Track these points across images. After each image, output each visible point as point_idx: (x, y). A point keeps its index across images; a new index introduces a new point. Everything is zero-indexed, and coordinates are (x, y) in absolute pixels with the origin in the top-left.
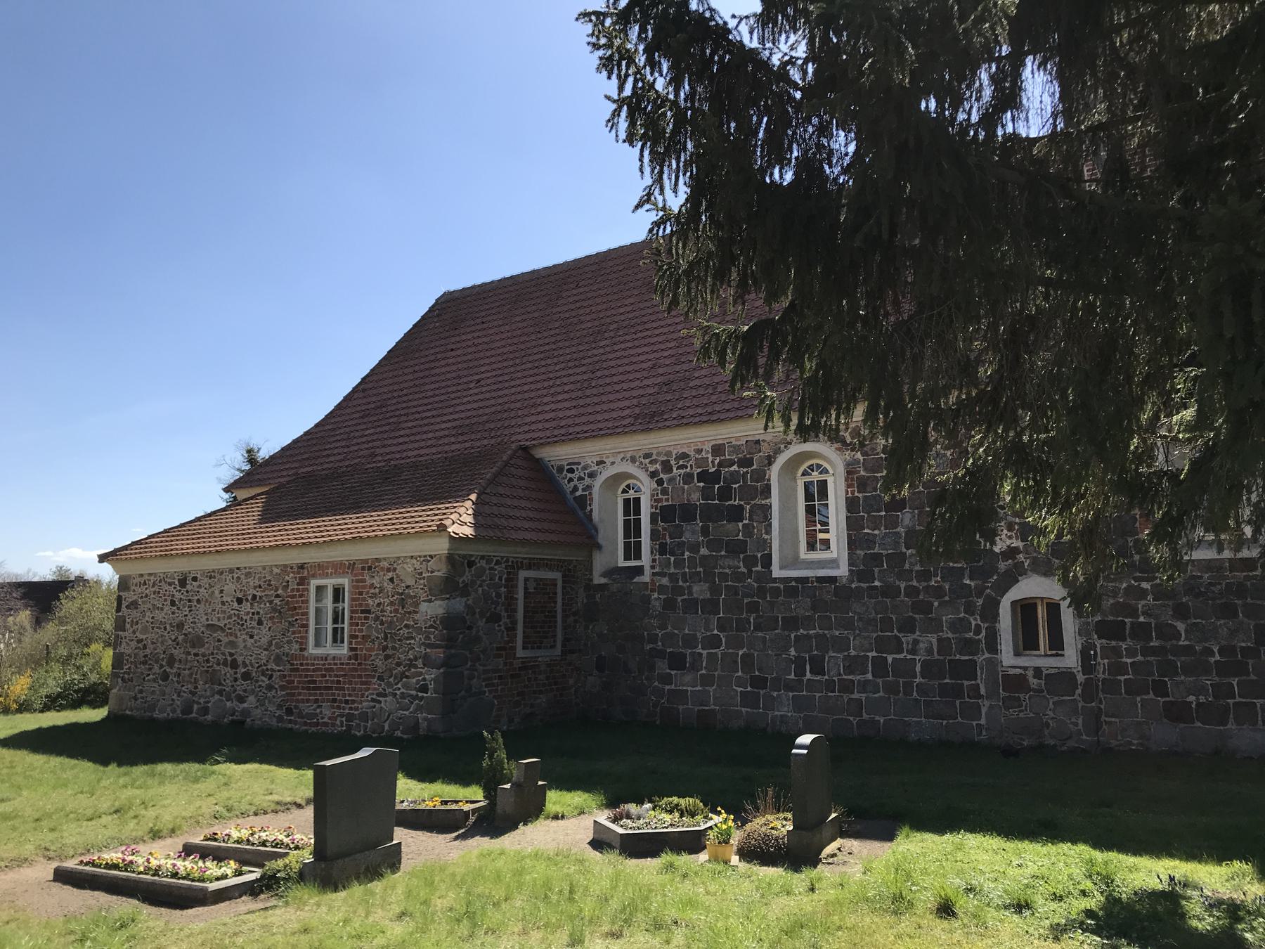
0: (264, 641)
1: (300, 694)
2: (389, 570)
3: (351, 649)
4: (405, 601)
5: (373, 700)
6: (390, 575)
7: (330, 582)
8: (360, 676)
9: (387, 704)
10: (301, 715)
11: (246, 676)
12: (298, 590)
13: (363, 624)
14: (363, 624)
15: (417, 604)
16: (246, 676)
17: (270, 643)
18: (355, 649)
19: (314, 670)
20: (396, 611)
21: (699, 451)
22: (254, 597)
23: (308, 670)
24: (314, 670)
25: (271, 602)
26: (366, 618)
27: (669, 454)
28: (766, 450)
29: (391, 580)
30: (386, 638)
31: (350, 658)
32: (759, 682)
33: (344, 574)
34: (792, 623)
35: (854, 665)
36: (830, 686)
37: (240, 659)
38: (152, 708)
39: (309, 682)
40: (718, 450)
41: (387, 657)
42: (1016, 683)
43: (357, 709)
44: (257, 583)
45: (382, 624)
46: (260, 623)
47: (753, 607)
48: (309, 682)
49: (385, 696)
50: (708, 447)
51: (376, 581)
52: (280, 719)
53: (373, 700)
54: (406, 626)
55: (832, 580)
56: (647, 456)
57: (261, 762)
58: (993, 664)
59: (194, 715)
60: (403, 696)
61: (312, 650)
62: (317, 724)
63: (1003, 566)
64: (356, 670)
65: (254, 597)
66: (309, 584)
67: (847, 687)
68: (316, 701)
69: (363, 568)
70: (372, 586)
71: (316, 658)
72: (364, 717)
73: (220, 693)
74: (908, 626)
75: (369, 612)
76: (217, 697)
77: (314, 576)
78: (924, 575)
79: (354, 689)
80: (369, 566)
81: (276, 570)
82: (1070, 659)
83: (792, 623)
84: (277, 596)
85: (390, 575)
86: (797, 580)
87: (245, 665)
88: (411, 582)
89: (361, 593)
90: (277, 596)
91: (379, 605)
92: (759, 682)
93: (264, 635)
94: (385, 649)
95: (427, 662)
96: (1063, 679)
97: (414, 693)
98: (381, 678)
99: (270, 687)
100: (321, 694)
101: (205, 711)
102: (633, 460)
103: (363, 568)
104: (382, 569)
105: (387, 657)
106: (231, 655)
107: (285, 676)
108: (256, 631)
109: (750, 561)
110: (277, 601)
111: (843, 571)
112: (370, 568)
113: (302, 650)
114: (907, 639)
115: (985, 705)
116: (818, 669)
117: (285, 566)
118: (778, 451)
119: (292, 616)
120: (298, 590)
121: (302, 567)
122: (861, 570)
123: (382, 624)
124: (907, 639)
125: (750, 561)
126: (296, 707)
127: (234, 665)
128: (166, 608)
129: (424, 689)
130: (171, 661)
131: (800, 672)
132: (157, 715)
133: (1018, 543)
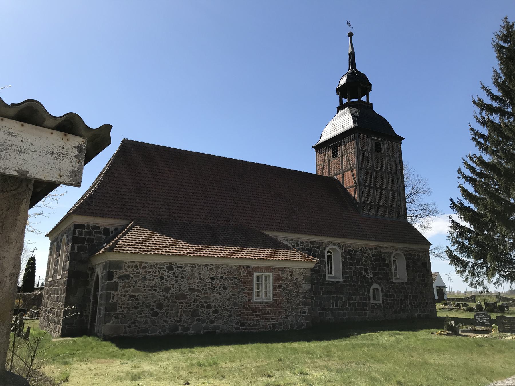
0: (228, 296)
1: (248, 317)
2: (290, 272)
3: (274, 299)
4: (295, 282)
5: (284, 318)
6: (290, 273)
7: (263, 275)
8: (278, 309)
9: (290, 318)
10: (249, 325)
11: (216, 312)
12: (247, 276)
13: (279, 290)
14: (279, 290)
15: (300, 284)
16: (216, 312)
17: (231, 297)
18: (276, 299)
19: (256, 308)
20: (293, 286)
21: (307, 242)
22: (222, 278)
23: (253, 308)
24: (256, 308)
25: (232, 280)
26: (280, 288)
27: (298, 241)
28: (324, 245)
29: (291, 275)
30: (288, 295)
31: (273, 303)
32: (323, 309)
33: (270, 272)
34: (331, 293)
35: (344, 304)
36: (339, 309)
37: (213, 305)
38: (145, 330)
39: (253, 312)
40: (312, 243)
41: (288, 302)
42: (373, 307)
43: (276, 321)
44: (223, 272)
45: (287, 290)
46: (225, 288)
47: (322, 289)
48: (253, 312)
49: (289, 316)
50: (309, 241)
51: (284, 275)
52: (237, 328)
53: (284, 318)
54: (296, 292)
55: (339, 282)
56: (292, 240)
57: (329, 339)
58: (369, 302)
59: (179, 331)
60: (296, 315)
61: (255, 299)
62: (258, 328)
63: (370, 281)
64: (276, 307)
65: (222, 278)
66: (253, 274)
67: (343, 310)
68: (258, 320)
69: (279, 270)
70: (283, 277)
71: (257, 303)
72: (280, 324)
73: (199, 320)
74: (354, 295)
75: (282, 286)
76: (196, 322)
77: (256, 271)
78: (357, 282)
79: (275, 314)
80: (282, 270)
81: (234, 267)
82: (381, 302)
83: (331, 293)
84: (235, 278)
85: (290, 273)
86: (332, 282)
87: (215, 306)
88: (298, 277)
89: (278, 279)
90: (235, 278)
91: (286, 284)
92: (323, 309)
93: (228, 294)
94: (288, 299)
95: (305, 304)
96: (379, 306)
97: (299, 314)
98: (286, 310)
99: (230, 316)
100: (260, 317)
101: (188, 329)
102: (287, 240)
103: (279, 270)
104: (287, 271)
105: (288, 302)
106: (206, 303)
107: (240, 311)
108: (222, 292)
109: (321, 276)
110: (236, 280)
111: (341, 280)
112: (282, 270)
113: (249, 300)
114: (354, 297)
115: (368, 312)
116: (337, 305)
117: (240, 266)
118: (326, 246)
119: (244, 286)
120: (247, 276)
121: (249, 267)
122: (345, 281)
123: (287, 290)
124: (354, 297)
125: (321, 276)
126: (246, 323)
127: (209, 307)
128: (156, 280)
129: (304, 312)
130: (160, 306)
131: (333, 306)
132: (149, 334)
133: (372, 276)
